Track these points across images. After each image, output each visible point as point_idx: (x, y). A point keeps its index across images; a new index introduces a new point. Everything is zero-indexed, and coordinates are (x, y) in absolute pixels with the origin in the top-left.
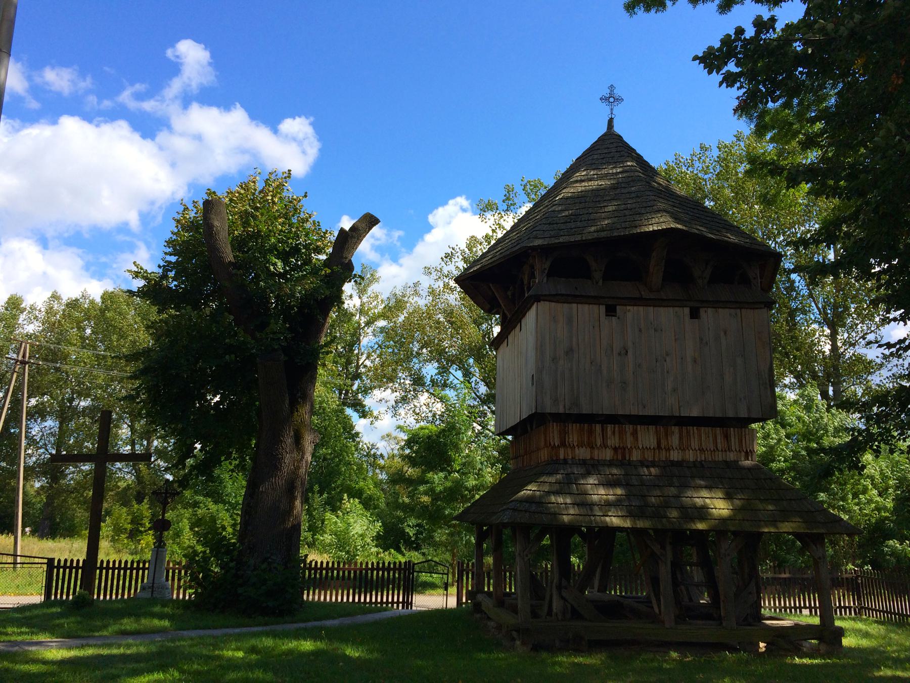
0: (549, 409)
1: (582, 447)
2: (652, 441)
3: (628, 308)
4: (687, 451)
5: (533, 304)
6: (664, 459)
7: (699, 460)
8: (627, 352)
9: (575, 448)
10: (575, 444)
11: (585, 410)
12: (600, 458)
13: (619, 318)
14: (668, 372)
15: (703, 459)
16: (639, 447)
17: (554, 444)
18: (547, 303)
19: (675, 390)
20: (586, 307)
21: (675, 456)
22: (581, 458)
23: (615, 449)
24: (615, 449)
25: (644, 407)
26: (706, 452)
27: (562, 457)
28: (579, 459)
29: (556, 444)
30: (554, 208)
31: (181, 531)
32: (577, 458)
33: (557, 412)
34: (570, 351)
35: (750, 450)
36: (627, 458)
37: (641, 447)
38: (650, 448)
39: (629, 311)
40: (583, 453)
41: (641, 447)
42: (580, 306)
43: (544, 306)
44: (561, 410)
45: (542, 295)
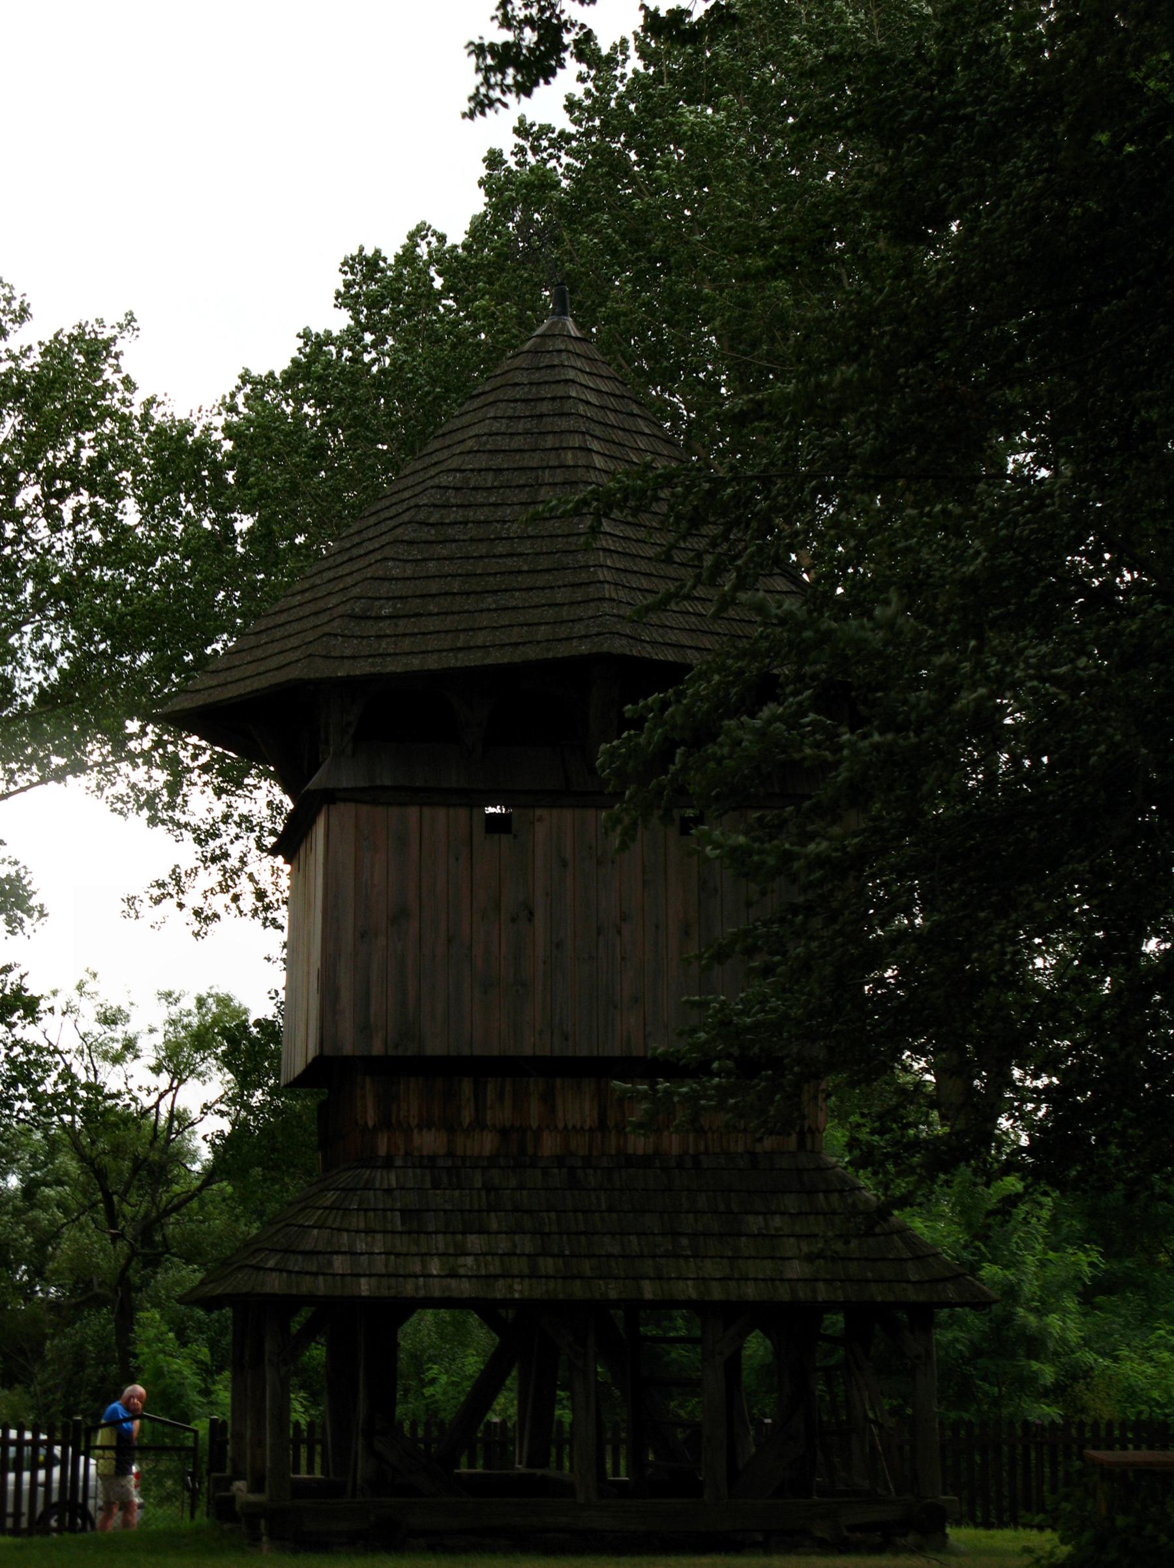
0: (349, 1046)
1: (430, 1129)
2: (587, 1112)
3: (538, 812)
4: (666, 1133)
5: (318, 813)
6: (613, 1152)
7: (691, 1151)
8: (531, 914)
9: (412, 1130)
10: (414, 1122)
11: (435, 1047)
12: (469, 1153)
13: (515, 837)
14: (623, 958)
15: (702, 1148)
16: (556, 1127)
17: (366, 1124)
18: (352, 806)
19: (362, 937)
20: (441, 813)
21: (639, 1144)
22: (425, 1153)
23: (504, 1133)
24: (504, 1133)
25: (567, 1039)
26: (709, 1135)
27: (382, 1151)
28: (422, 1157)
29: (370, 1124)
30: (399, 531)
31: (202, 431)
32: (416, 1153)
33: (366, 1053)
34: (399, 916)
35: (810, 1128)
36: (530, 1151)
37: (561, 1126)
38: (582, 1128)
39: (540, 819)
40: (430, 1142)
41: (561, 1126)
42: (427, 811)
43: (345, 812)
44: (377, 1049)
45: (339, 790)
